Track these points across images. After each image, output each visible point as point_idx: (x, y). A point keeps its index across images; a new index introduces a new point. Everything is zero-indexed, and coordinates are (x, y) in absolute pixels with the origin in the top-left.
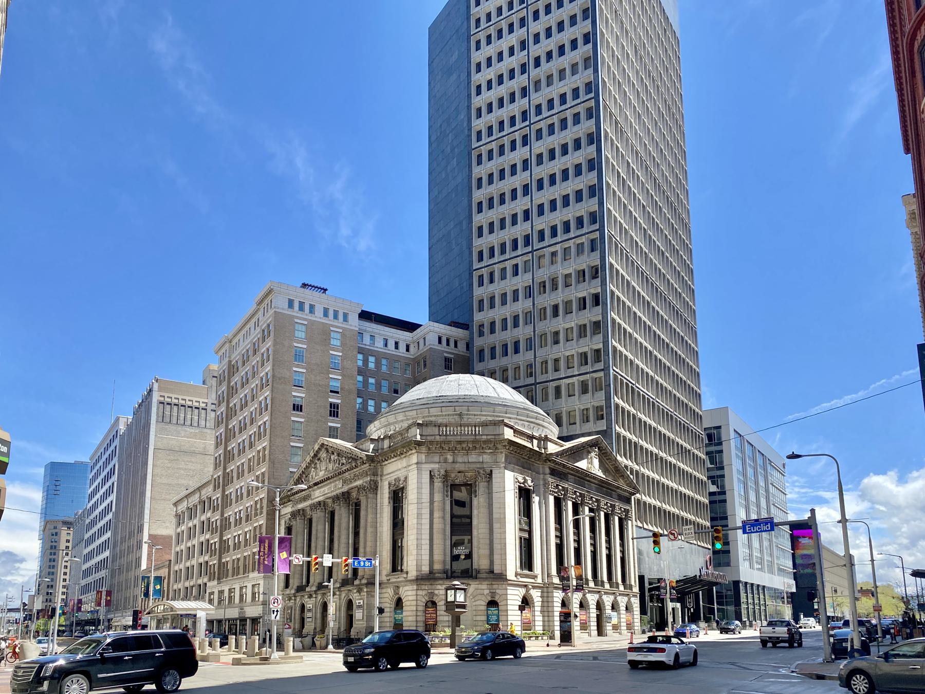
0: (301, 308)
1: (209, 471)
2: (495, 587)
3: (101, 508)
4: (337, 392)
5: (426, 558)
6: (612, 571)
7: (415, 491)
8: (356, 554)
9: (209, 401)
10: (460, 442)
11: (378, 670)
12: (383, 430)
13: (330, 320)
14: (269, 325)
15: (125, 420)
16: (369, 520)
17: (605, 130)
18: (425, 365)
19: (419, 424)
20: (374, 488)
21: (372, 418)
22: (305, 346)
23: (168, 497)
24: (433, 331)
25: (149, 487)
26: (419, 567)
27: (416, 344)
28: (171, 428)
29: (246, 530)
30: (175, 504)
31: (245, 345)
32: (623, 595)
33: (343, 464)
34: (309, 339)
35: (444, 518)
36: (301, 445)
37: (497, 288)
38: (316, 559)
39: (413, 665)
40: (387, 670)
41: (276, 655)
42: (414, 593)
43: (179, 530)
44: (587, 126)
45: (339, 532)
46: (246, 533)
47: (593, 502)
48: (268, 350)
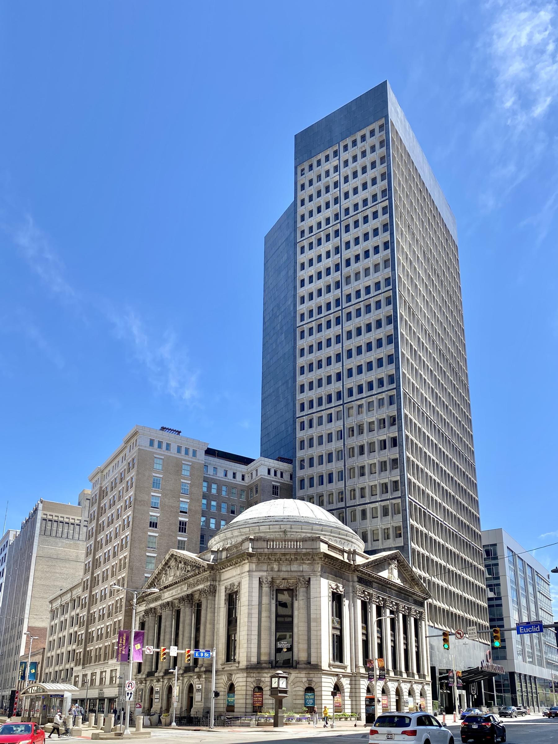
0: (160, 446)
2: (312, 675)
4: (186, 513)
5: (255, 650)
6: (410, 663)
7: (247, 594)
8: (197, 646)
10: (284, 554)
12: (221, 544)
13: (182, 455)
14: (133, 459)
16: (208, 618)
17: (400, 313)
18: (257, 492)
20: (213, 591)
21: (213, 534)
22: (161, 476)
27: (250, 475)
29: (108, 624)
30: (51, 602)
31: (114, 475)
32: (418, 683)
33: (188, 571)
35: (270, 617)
36: (155, 555)
38: (164, 649)
41: (129, 731)
42: (245, 679)
43: (53, 623)
44: (387, 310)
45: (184, 627)
47: (393, 605)
48: (132, 478)
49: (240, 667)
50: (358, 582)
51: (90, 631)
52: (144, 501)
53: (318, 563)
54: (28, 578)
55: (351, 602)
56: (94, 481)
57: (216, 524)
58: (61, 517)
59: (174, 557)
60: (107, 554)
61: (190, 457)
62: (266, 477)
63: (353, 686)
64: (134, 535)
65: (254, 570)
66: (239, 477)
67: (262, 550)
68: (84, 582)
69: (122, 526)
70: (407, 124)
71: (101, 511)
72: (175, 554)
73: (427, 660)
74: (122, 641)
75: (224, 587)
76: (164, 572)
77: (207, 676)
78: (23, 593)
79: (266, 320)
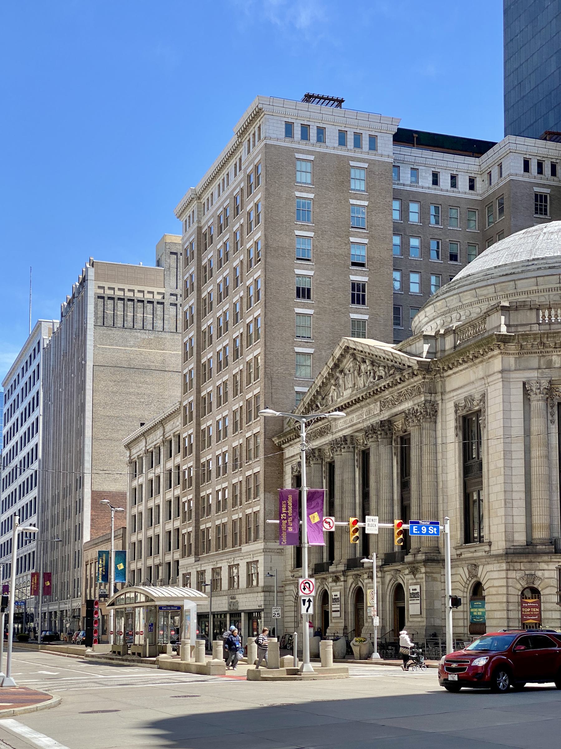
0: (305, 135)
1: (174, 395)
3: (22, 455)
4: (362, 265)
5: (520, 520)
7: (500, 416)
8: (405, 516)
9: (167, 291)
11: (495, 690)
12: (439, 321)
13: (349, 150)
14: (257, 167)
15: (50, 323)
16: (425, 463)
18: (501, 210)
19: (503, 308)
20: (431, 412)
21: (420, 303)
22: (312, 196)
23: (115, 435)
24: (514, 156)
25: (88, 422)
26: (509, 535)
27: (486, 176)
28: (116, 333)
29: (234, 481)
30: (128, 446)
31: (220, 202)
33: (380, 377)
34: (318, 182)
35: (548, 457)
36: (311, 351)
38: (355, 522)
39: (553, 684)
40: (508, 691)
41: (310, 667)
42: (503, 574)
43: (135, 484)
45: (377, 482)
46: (234, 486)
48: (257, 205)
49: (492, 553)
51: (202, 494)
52: (283, 248)
54: (83, 406)
56: (185, 217)
57: (402, 282)
58: (109, 288)
59: (351, 351)
60: (222, 353)
61: (365, 152)
62: (521, 179)
64: (269, 315)
65: (513, 368)
66: (445, 181)
67: (528, 328)
68: (185, 407)
69: (245, 300)
71: (203, 274)
72: (352, 346)
74: (287, 509)
75: (453, 405)
76: (333, 381)
77: (428, 570)
78: (77, 434)
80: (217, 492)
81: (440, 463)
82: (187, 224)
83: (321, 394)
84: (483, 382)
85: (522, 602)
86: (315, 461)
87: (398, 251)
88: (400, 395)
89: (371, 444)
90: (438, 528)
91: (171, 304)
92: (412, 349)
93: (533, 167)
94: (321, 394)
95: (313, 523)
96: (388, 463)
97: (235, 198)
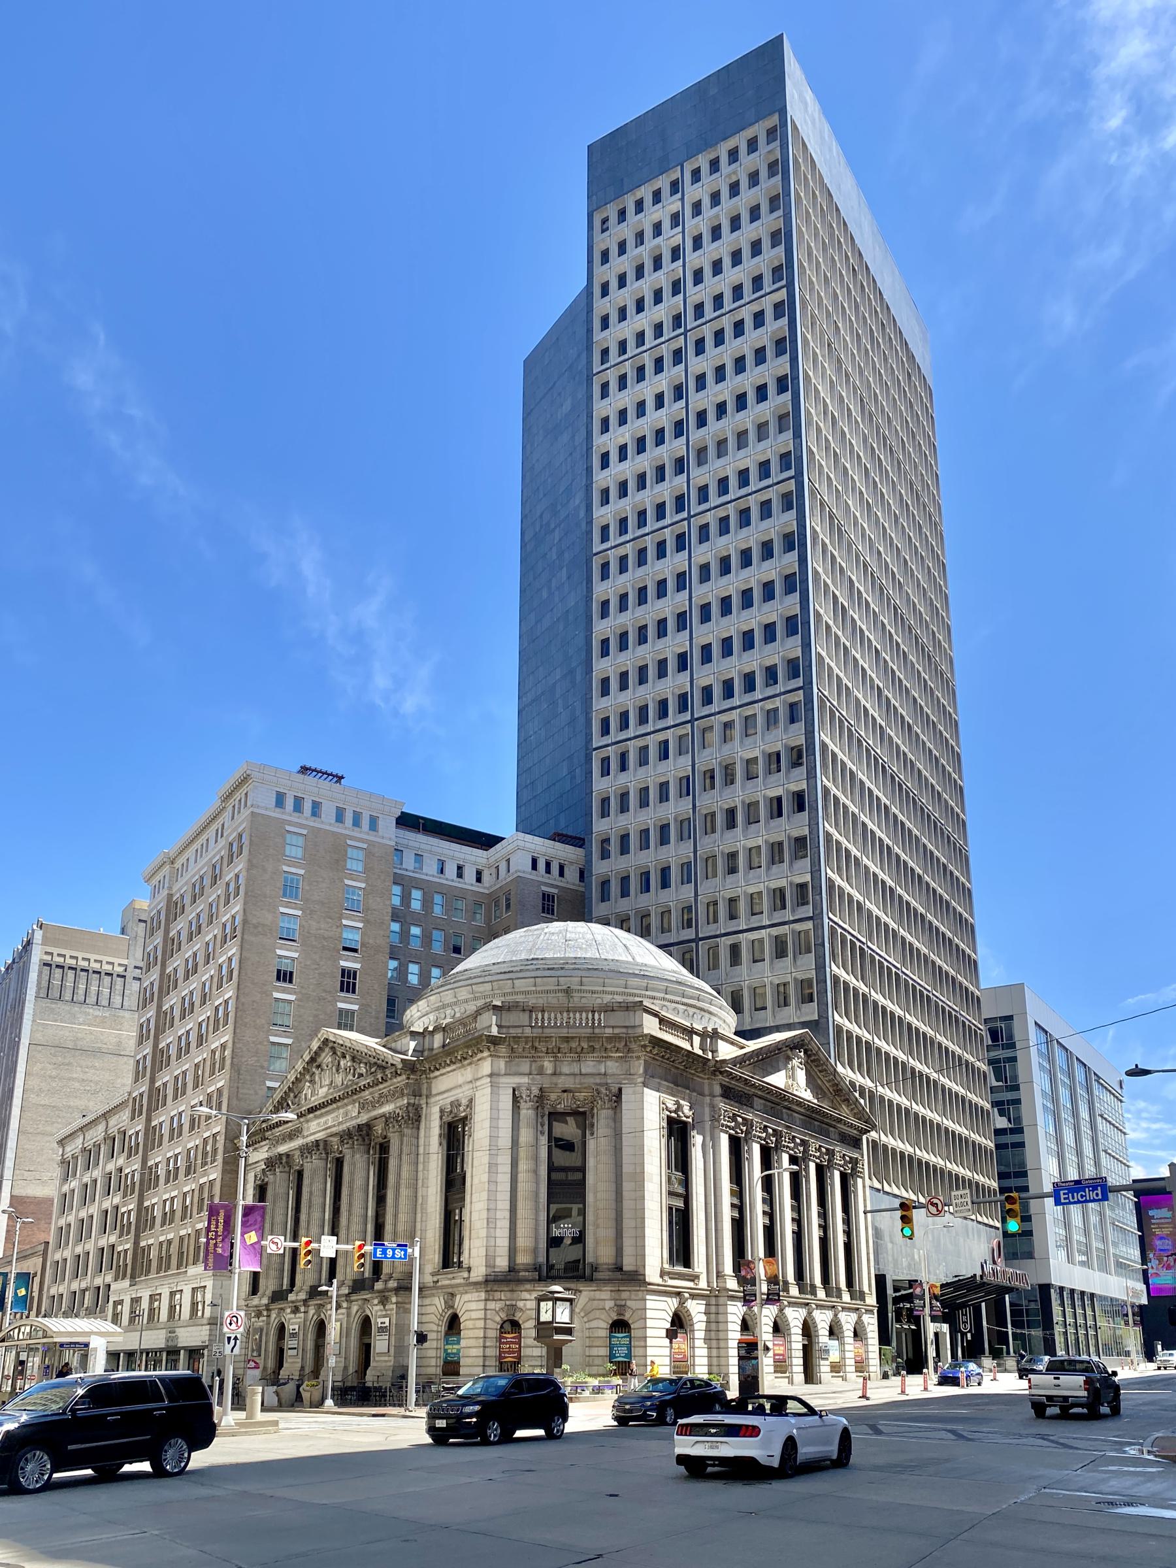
1: (122, 1082)
2: (625, 1295)
4: (355, 951)
5: (503, 1242)
6: (828, 1267)
7: (487, 1124)
8: (379, 1235)
9: (130, 962)
10: (567, 1039)
11: (486, 1442)
12: (432, 1017)
17: (812, 528)
18: (508, 906)
19: (495, 1007)
20: (414, 1117)
21: (414, 995)
22: (302, 872)
23: (48, 1129)
27: (494, 871)
30: (62, 1142)
31: (197, 868)
33: (361, 1075)
35: (535, 1172)
37: (632, 780)
42: (481, 1305)
43: (66, 1188)
44: (784, 521)
45: (350, 1195)
47: (796, 1145)
48: (237, 876)
49: (471, 1280)
50: (722, 1096)
51: (146, 1204)
53: (638, 1058)
55: (708, 1138)
56: (154, 881)
59: (331, 1045)
63: (713, 1316)
64: (242, 999)
65: (503, 1072)
67: (520, 1030)
69: (215, 980)
70: (827, 128)
73: (868, 1260)
76: (308, 1077)
77: (400, 1300)
79: (527, 539)
80: (165, 1201)
81: (420, 1175)
82: (155, 891)
83: (294, 1090)
84: (471, 1086)
85: (501, 1337)
86: (281, 1169)
87: (395, 939)
88: (381, 1096)
89: (347, 1152)
90: (406, 1251)
91: (134, 978)
92: (398, 1045)
93: (541, 865)
94: (294, 1090)
95: (248, 1243)
96: (364, 1174)
97: (214, 866)
